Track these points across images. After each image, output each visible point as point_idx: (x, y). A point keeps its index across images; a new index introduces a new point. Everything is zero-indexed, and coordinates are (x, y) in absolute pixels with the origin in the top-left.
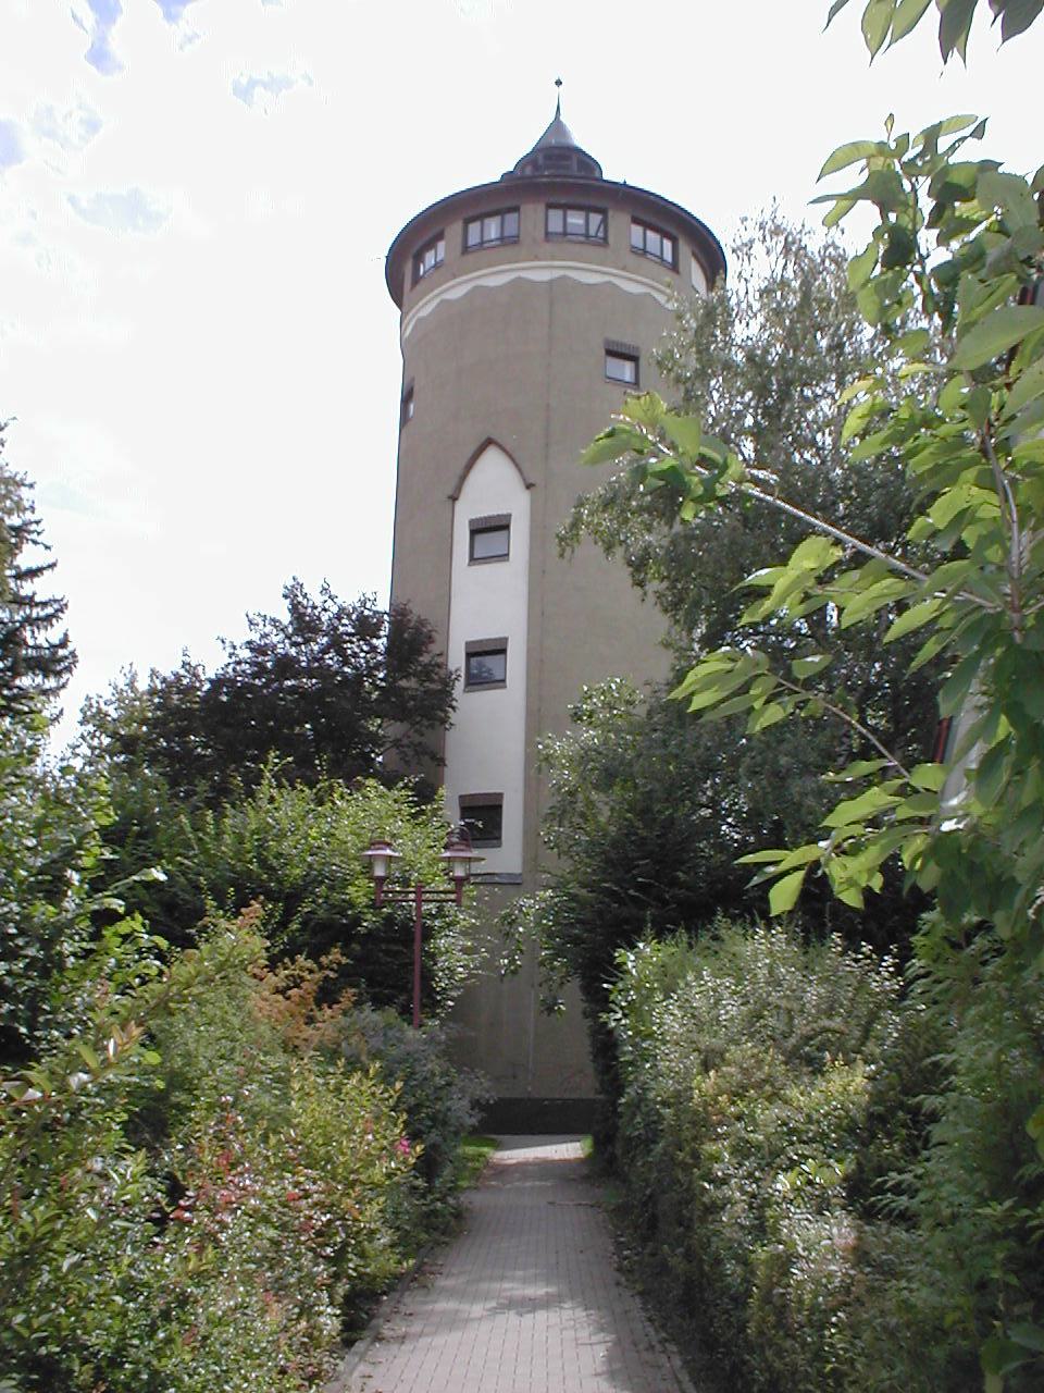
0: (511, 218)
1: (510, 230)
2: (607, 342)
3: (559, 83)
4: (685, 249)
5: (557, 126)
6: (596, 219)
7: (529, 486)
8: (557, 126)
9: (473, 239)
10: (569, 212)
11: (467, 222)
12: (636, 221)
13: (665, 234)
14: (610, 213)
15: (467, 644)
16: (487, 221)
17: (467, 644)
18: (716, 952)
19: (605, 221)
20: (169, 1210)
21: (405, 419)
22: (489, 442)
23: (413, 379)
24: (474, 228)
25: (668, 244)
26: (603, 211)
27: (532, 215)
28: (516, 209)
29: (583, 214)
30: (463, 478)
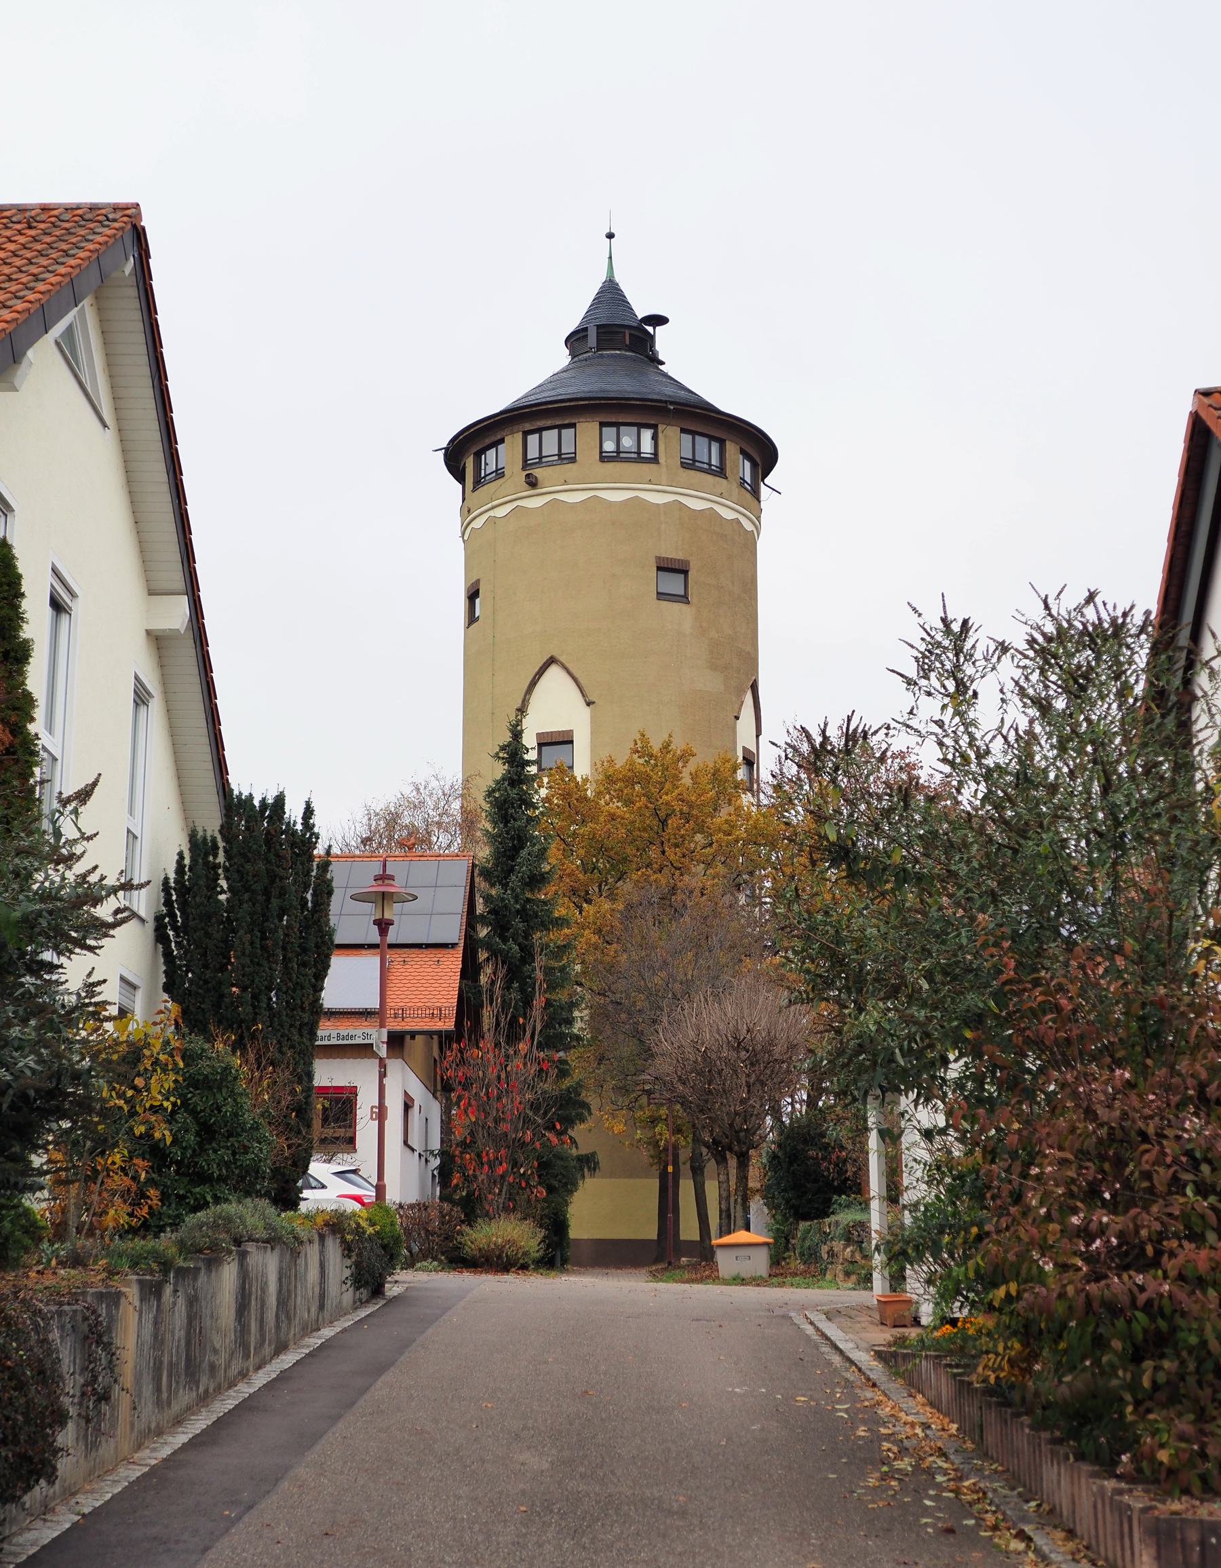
0: (567, 433)
1: (567, 448)
2: (658, 559)
3: (610, 236)
4: (732, 449)
5: (611, 294)
6: (647, 435)
7: (588, 704)
8: (611, 294)
9: (533, 453)
10: (622, 428)
11: (526, 434)
12: (683, 431)
13: (712, 438)
14: (661, 428)
15: (538, 734)
16: (544, 433)
17: (538, 734)
18: (505, 1521)
19: (655, 438)
20: (1162, 1426)
21: (472, 619)
22: (552, 661)
23: (478, 581)
24: (533, 439)
25: (715, 447)
26: (654, 427)
27: (587, 435)
28: (573, 426)
29: (635, 429)
30: (533, 683)
